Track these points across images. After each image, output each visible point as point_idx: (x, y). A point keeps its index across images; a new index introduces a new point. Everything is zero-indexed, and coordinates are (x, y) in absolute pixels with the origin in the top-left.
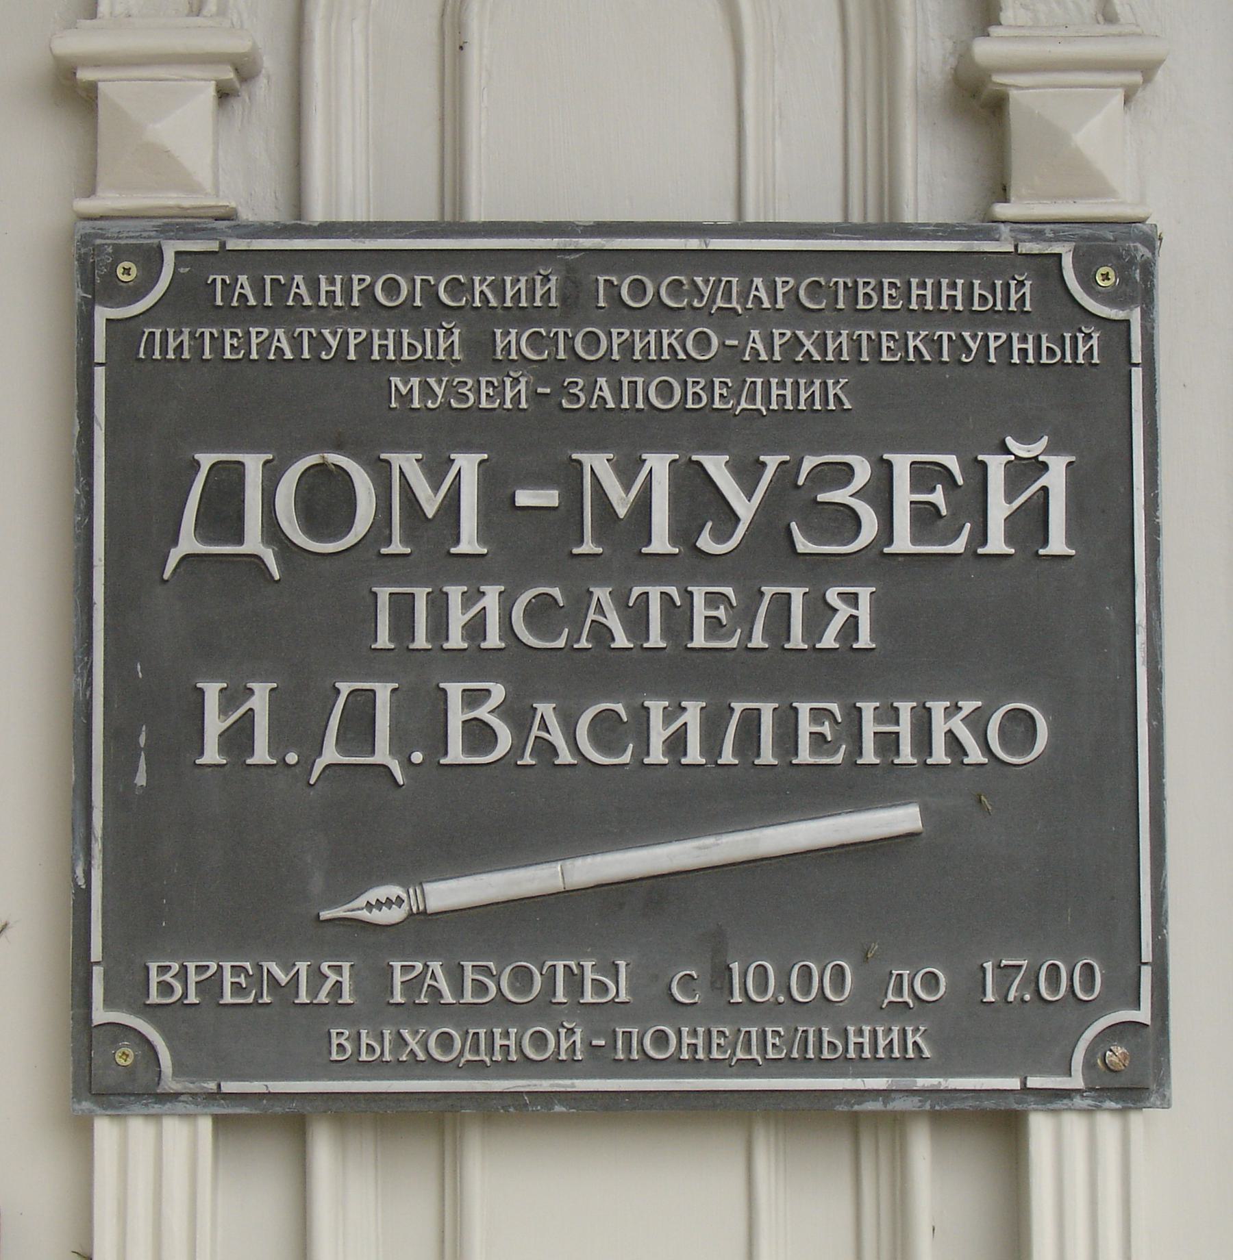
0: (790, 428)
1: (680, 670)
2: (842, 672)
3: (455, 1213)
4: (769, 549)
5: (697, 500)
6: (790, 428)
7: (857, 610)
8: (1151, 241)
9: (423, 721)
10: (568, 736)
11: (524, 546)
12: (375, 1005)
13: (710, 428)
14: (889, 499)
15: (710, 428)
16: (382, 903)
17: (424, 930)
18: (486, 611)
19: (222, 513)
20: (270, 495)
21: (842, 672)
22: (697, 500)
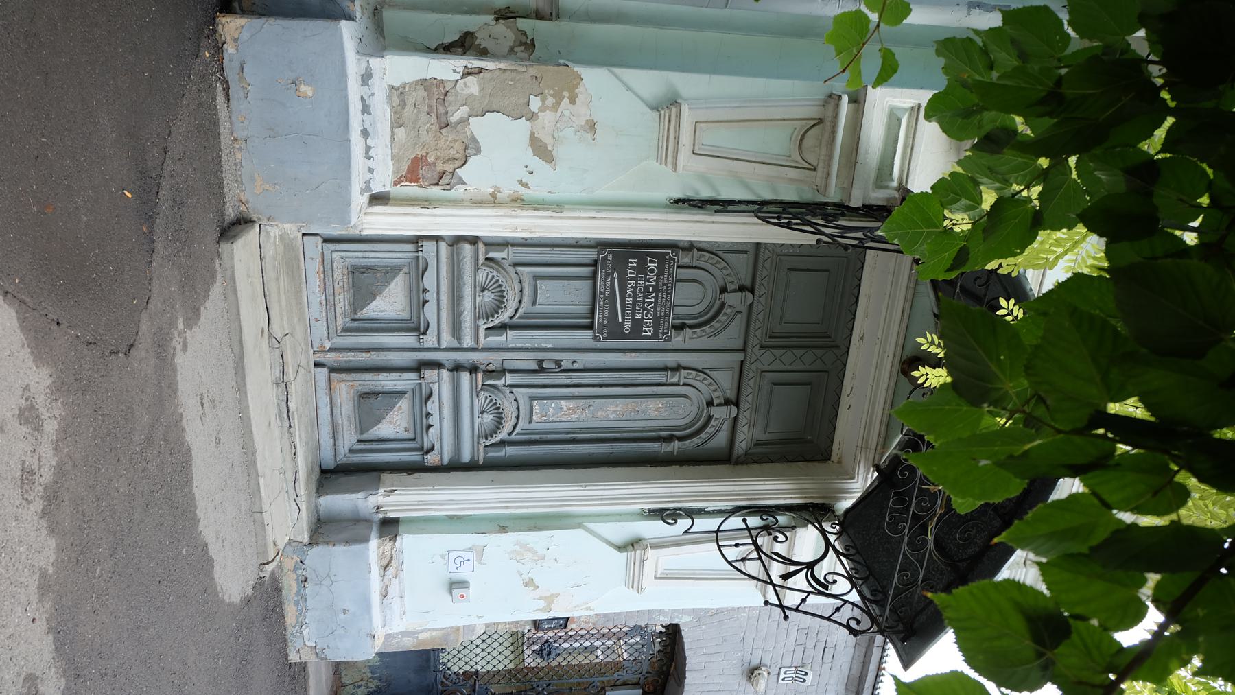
0: (655, 312)
1: (634, 301)
2: (633, 315)
3: (620, 514)
4: (644, 309)
5: (650, 303)
6: (655, 312)
7: (639, 316)
8: (895, 71)
9: (632, 279)
10: (629, 292)
11: (646, 288)
12: (607, 274)
13: (656, 302)
14: (648, 320)
15: (656, 302)
16: (616, 275)
17: (613, 279)
18: (641, 285)
19: (651, 262)
20: (653, 266)
21: (633, 315)
22: (650, 303)
